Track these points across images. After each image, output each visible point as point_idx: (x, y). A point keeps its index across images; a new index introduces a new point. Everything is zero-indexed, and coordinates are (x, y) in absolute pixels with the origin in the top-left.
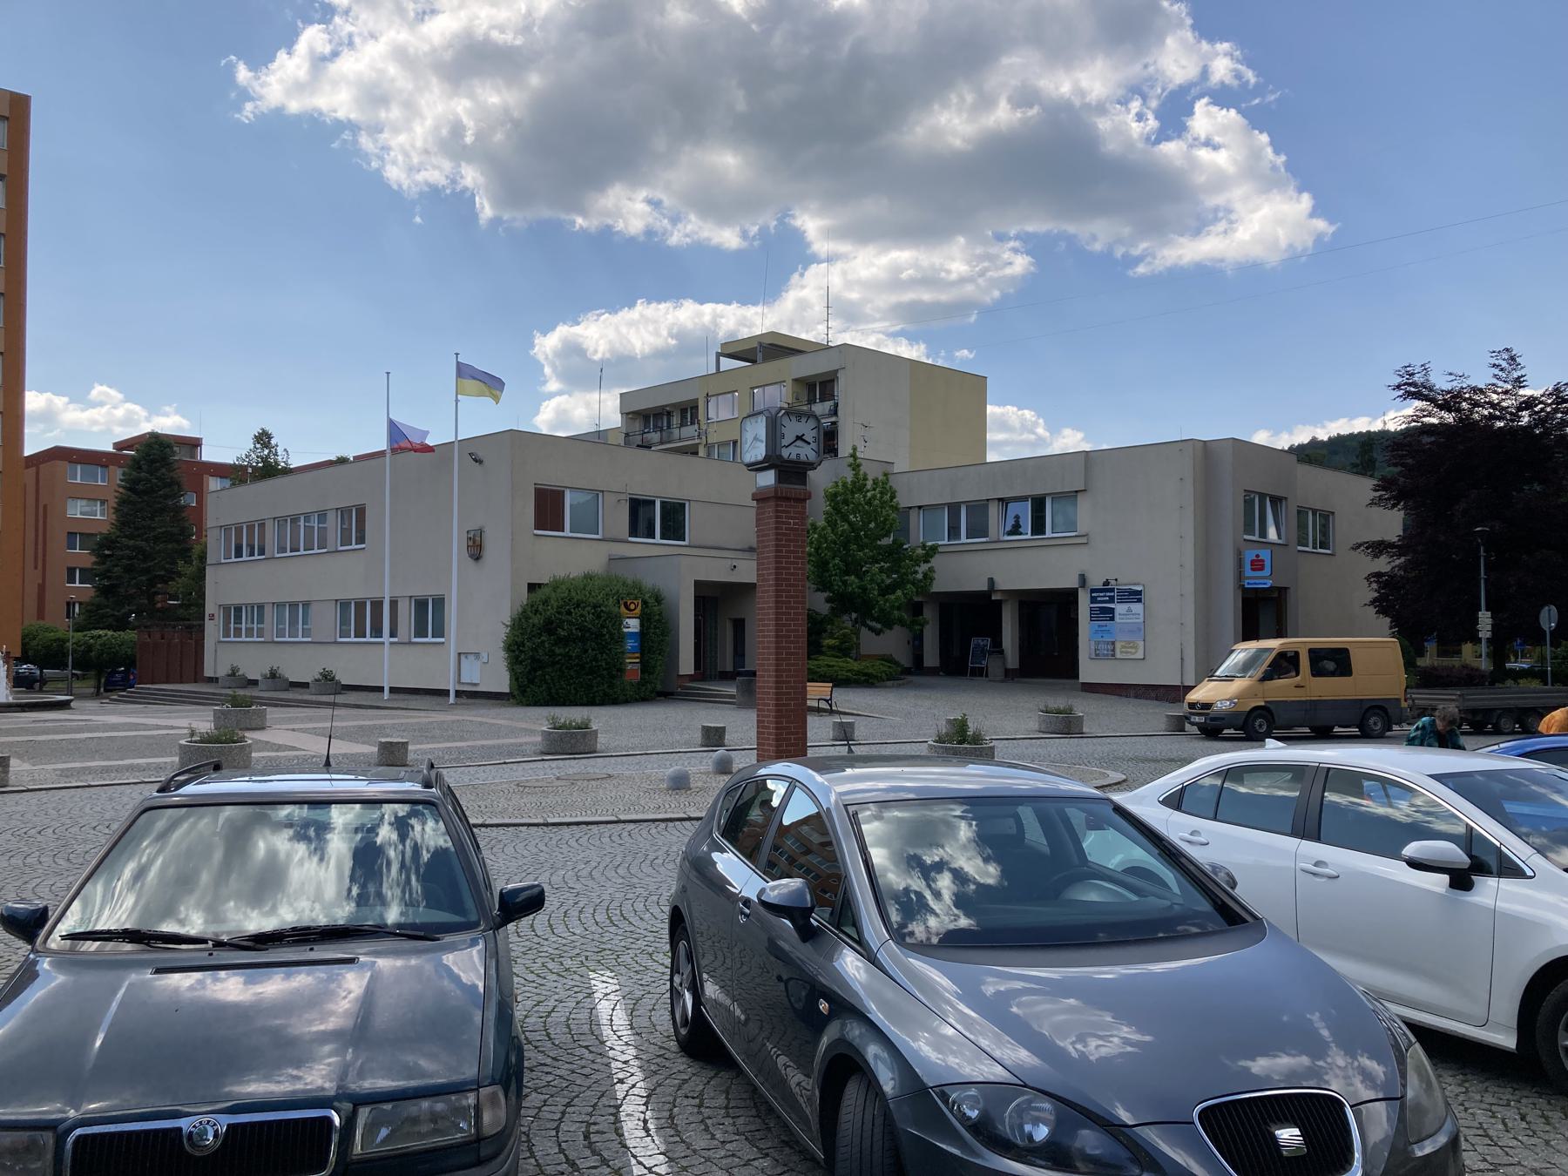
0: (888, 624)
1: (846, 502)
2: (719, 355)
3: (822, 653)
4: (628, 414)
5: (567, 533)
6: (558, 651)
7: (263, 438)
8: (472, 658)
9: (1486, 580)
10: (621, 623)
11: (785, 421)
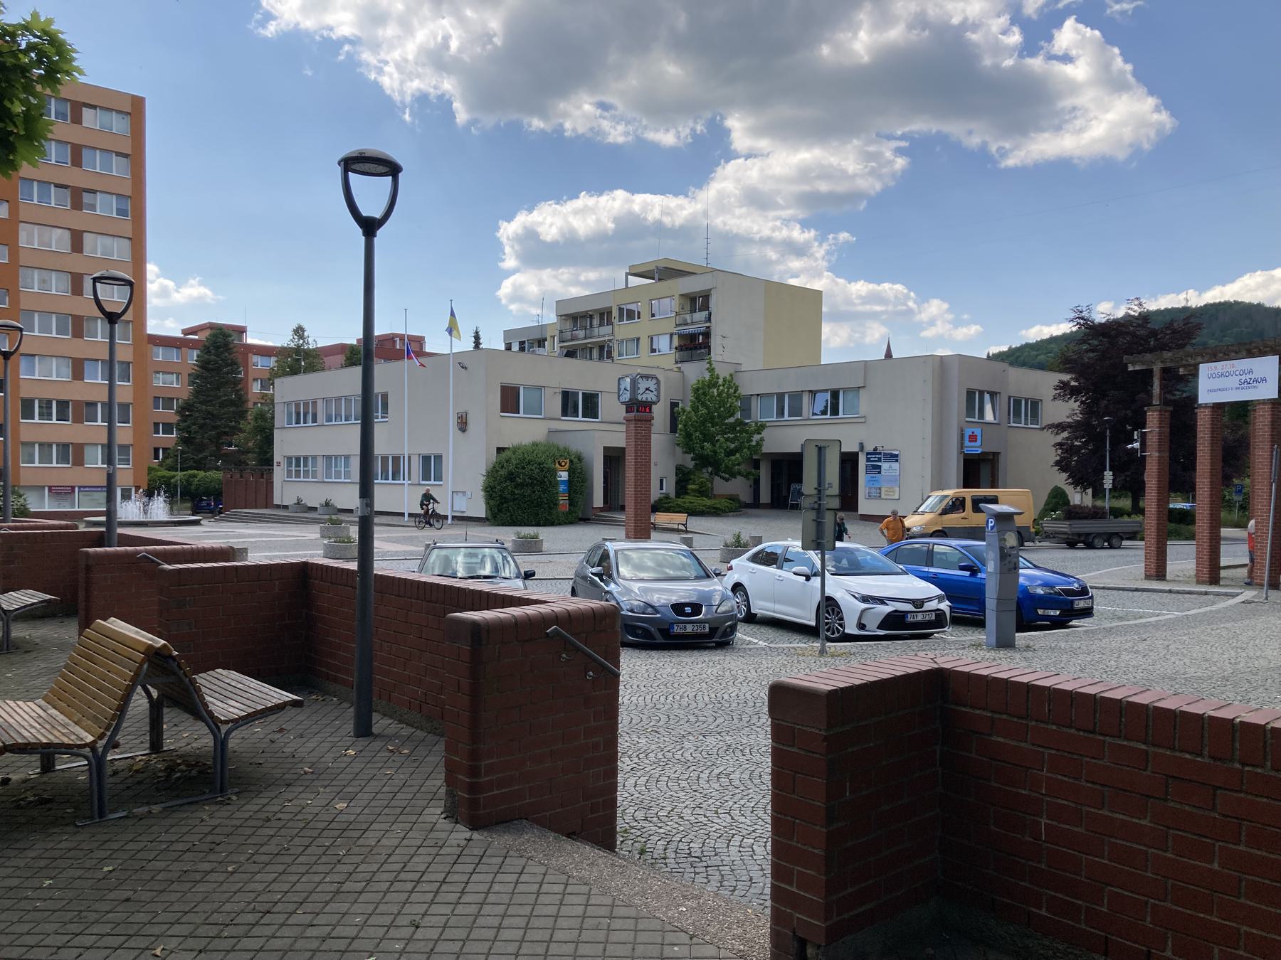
0: (733, 475)
1: (704, 394)
2: (627, 274)
3: (687, 493)
4: (561, 316)
5: (521, 414)
6: (516, 492)
7: (299, 331)
8: (460, 495)
9: (1110, 451)
10: (556, 474)
11: (640, 380)
